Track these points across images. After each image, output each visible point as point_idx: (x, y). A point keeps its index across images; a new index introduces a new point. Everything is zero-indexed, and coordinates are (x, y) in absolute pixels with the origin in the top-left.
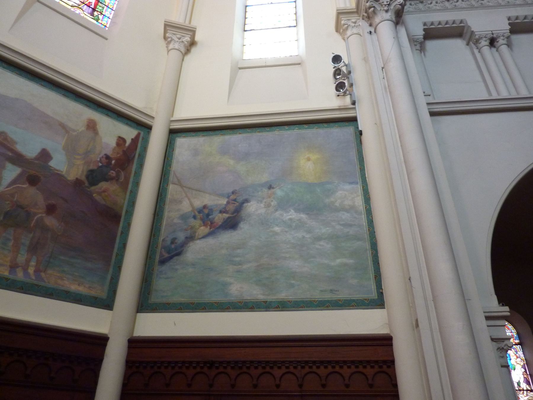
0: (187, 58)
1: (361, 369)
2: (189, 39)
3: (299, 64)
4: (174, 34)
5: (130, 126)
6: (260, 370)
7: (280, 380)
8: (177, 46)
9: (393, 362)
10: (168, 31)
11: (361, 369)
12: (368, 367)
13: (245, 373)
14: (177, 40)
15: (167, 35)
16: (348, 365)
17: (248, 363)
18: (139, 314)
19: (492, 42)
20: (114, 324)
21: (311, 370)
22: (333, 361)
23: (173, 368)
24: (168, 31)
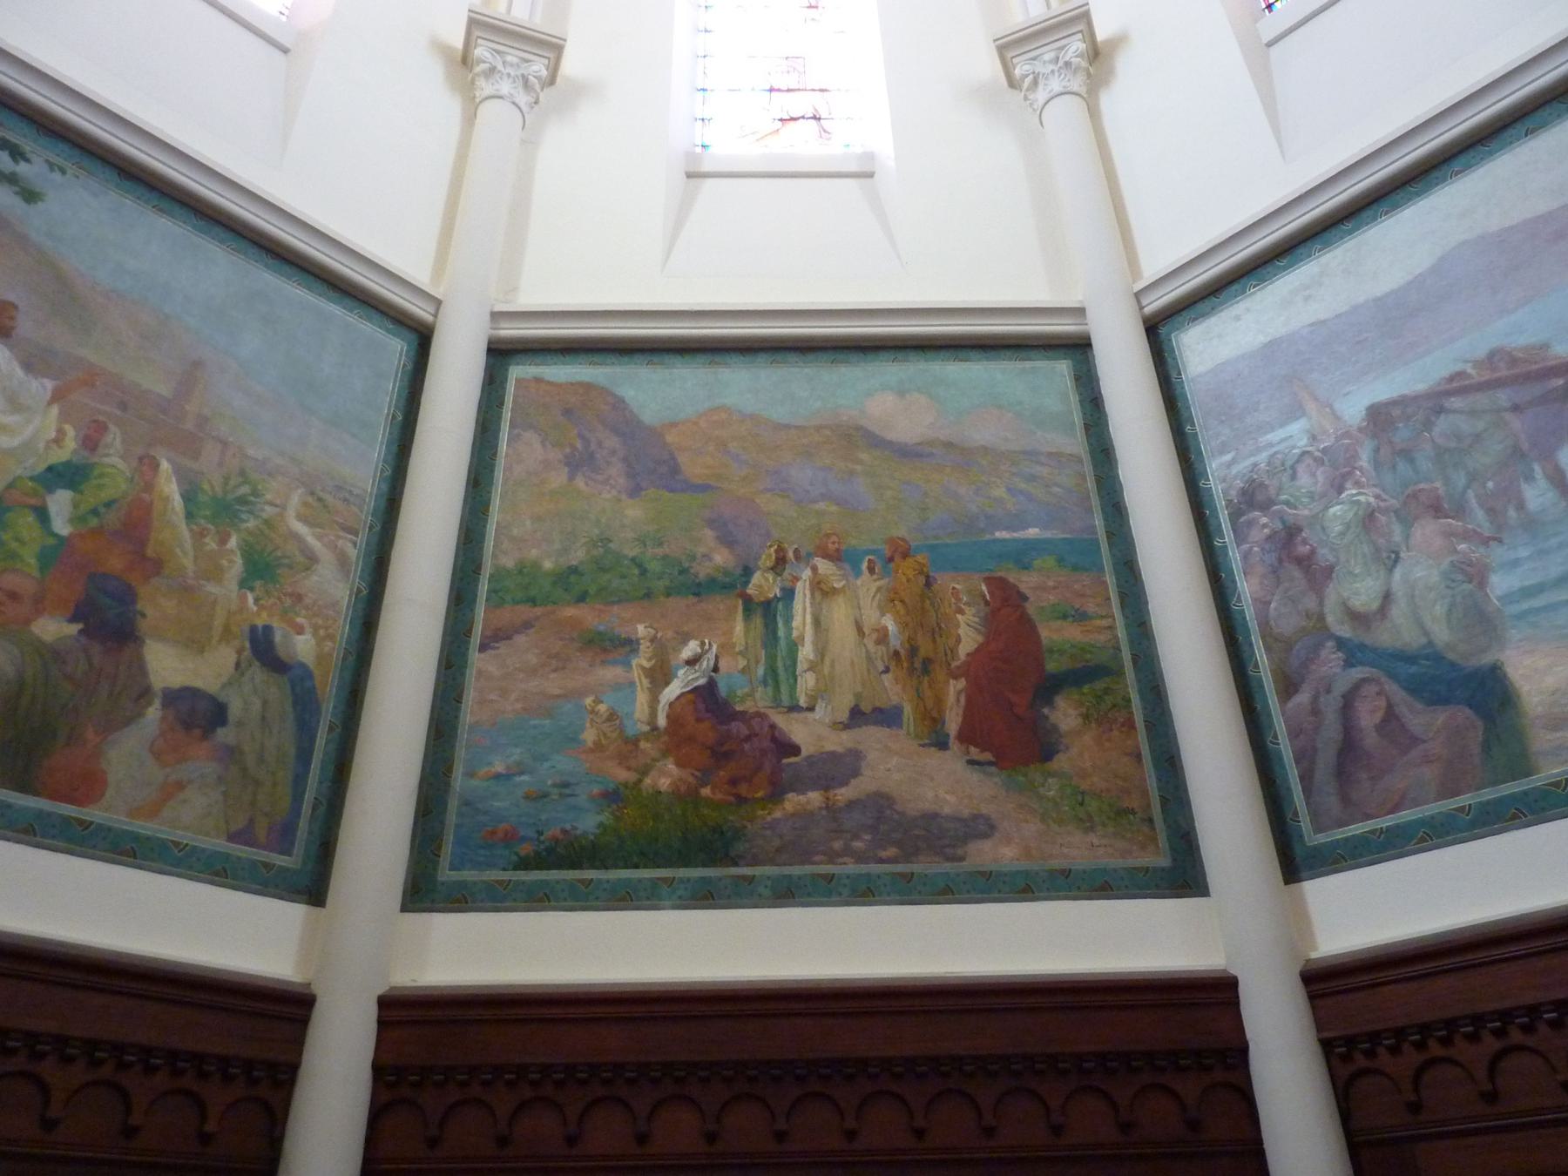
0: (1109, 101)
2: (1082, 46)
4: (1034, 59)
5: (1543, 126)
6: (1491, 1044)
7: (1416, 1090)
8: (1056, 85)
9: (1242, 1051)
13: (1520, 1048)
14: (1051, 67)
15: (1018, 72)
20: (1239, 927)
22: (1519, 1008)
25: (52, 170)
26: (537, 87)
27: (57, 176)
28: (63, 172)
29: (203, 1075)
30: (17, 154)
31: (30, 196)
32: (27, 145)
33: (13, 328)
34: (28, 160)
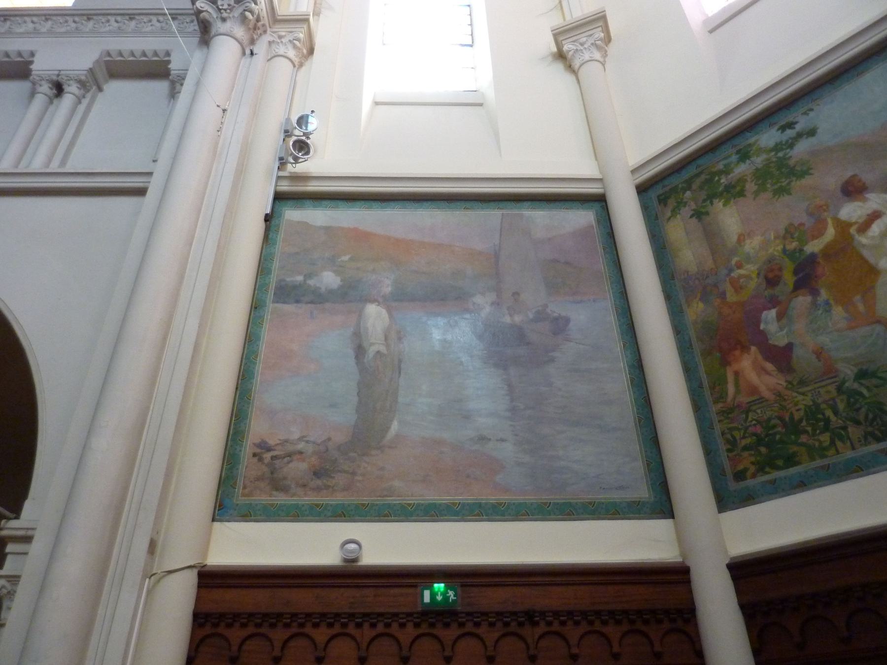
1: (597, 626)
3: (481, 105)
7: (325, 650)
10: (564, 42)
11: (597, 626)
12: (570, 623)
16: (686, 616)
17: (401, 616)
18: (217, 525)
19: (59, 89)
21: (387, 631)
23: (373, 626)
24: (564, 42)
25: (808, 114)
26: (603, 45)
27: (812, 114)
28: (812, 110)
29: (646, 622)
30: (790, 125)
31: (812, 133)
32: (790, 119)
33: (864, 184)
34: (796, 123)
